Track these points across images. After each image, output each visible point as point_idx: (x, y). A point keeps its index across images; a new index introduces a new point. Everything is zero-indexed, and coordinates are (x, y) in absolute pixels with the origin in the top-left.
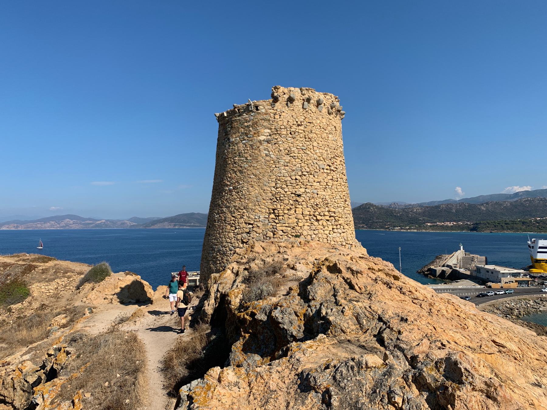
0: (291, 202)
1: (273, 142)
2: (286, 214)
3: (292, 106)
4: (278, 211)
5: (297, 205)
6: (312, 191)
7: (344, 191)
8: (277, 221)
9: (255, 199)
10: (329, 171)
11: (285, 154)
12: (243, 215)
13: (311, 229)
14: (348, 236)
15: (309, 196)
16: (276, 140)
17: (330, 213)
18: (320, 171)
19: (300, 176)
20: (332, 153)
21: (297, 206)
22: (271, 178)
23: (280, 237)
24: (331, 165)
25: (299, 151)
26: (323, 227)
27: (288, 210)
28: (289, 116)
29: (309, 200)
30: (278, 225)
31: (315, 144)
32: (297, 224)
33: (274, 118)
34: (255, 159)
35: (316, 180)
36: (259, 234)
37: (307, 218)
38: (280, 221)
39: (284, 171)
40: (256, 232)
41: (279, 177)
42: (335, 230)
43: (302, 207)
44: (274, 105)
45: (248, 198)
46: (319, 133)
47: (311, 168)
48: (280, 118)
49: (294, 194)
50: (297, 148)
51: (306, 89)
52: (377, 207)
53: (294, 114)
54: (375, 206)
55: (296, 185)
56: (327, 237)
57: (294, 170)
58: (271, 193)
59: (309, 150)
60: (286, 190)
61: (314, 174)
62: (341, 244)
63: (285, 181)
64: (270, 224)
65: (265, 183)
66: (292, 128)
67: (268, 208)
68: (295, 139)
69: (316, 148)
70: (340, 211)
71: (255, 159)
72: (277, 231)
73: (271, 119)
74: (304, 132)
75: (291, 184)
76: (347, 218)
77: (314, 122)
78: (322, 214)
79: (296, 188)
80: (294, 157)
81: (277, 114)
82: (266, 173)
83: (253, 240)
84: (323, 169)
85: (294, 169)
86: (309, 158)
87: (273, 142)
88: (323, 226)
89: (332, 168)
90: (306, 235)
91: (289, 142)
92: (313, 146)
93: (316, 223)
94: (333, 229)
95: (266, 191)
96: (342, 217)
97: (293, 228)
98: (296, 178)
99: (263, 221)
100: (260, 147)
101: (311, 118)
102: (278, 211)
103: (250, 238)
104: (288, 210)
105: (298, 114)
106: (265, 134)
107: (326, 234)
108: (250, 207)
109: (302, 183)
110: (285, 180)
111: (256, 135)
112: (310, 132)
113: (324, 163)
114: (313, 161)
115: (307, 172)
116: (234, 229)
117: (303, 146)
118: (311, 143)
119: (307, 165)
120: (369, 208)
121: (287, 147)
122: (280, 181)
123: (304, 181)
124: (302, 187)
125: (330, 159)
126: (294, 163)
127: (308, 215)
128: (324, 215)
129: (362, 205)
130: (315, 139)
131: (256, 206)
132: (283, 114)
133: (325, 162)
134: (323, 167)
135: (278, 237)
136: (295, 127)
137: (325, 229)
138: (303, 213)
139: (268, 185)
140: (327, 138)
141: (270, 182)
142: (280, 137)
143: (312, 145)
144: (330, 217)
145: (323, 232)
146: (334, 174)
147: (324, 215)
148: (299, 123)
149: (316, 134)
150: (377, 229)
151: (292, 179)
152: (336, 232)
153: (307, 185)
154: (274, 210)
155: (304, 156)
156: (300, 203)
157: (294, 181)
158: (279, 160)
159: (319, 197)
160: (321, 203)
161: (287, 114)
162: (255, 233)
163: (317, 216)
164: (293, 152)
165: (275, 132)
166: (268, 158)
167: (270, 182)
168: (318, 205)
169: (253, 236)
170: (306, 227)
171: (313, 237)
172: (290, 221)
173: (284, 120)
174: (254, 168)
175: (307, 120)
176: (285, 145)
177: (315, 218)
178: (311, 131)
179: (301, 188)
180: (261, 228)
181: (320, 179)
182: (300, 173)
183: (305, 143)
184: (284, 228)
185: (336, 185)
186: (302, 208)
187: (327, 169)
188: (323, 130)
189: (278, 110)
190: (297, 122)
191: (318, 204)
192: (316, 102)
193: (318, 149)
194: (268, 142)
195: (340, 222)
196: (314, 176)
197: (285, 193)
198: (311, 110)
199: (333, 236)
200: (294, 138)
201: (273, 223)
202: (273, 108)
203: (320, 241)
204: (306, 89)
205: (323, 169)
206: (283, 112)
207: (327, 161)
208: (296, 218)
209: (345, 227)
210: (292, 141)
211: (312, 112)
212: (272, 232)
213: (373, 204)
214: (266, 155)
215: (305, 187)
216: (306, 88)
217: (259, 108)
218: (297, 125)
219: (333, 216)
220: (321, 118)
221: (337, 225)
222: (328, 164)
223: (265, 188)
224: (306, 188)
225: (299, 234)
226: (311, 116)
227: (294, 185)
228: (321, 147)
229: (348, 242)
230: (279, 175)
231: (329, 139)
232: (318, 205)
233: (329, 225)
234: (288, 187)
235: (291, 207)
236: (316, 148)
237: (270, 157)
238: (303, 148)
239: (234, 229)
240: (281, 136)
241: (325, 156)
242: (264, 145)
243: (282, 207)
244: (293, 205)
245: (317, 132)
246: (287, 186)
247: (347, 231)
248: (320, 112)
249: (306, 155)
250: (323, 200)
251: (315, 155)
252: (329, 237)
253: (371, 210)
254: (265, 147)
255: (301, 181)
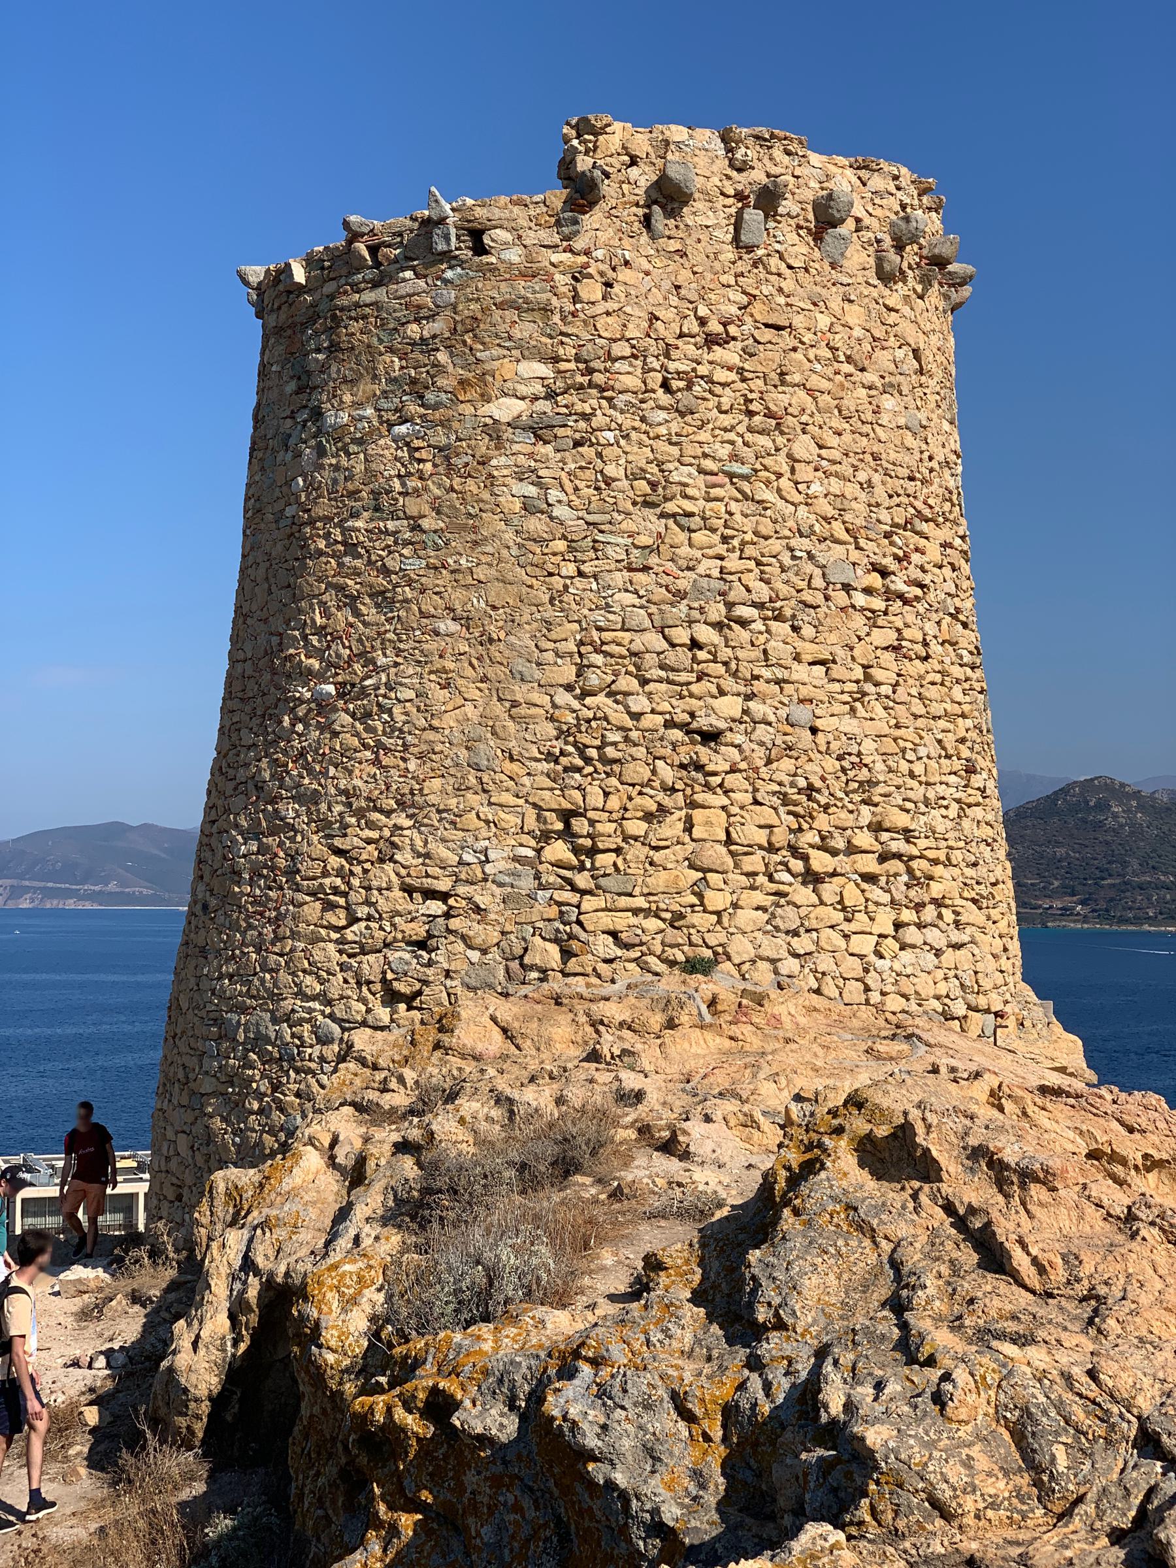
0: (667, 773)
1: (569, 432)
2: (636, 839)
3: (673, 233)
4: (592, 823)
5: (698, 788)
6: (782, 713)
7: (963, 716)
8: (583, 880)
9: (463, 754)
10: (878, 604)
11: (634, 504)
12: (394, 845)
13: (777, 929)
14: (980, 967)
15: (767, 739)
16: (582, 425)
17: (885, 836)
18: (827, 598)
19: (718, 626)
20: (896, 500)
21: (699, 798)
22: (553, 636)
23: (603, 968)
24: (893, 566)
25: (714, 486)
26: (841, 915)
27: (648, 817)
28: (659, 287)
29: (769, 762)
30: (589, 903)
31: (803, 447)
32: (700, 896)
33: (576, 299)
34: (464, 527)
35: (809, 651)
36: (484, 952)
37: (754, 862)
38: (602, 881)
39: (630, 598)
40: (463, 938)
41: (599, 629)
42: (912, 935)
43: (725, 801)
44: (576, 222)
45: (424, 747)
46: (825, 385)
47: (779, 585)
48: (604, 298)
49: (685, 727)
50: (701, 471)
51: (757, 137)
52: (1146, 803)
53: (684, 276)
54: (1137, 794)
55: (692, 677)
56: (866, 971)
57: (681, 595)
58: (552, 719)
59: (768, 483)
60: (639, 703)
61: (794, 616)
62: (943, 1013)
63: (635, 654)
64: (548, 894)
65: (520, 665)
66: (674, 354)
67: (535, 806)
68: (688, 418)
69: (810, 468)
70: (941, 826)
71: (464, 527)
72: (583, 936)
73: (555, 301)
74: (744, 380)
75: (663, 674)
76: (975, 865)
77: (798, 321)
78: (839, 843)
79: (691, 695)
80: (684, 521)
81: (590, 276)
82: (527, 610)
83: (449, 983)
84: (847, 588)
85: (682, 584)
86: (766, 527)
87: (569, 432)
88: (844, 909)
89: (899, 585)
90: (746, 957)
91: (658, 437)
92: (790, 456)
93: (803, 894)
94: (898, 926)
95: (523, 710)
96: (948, 863)
97: (677, 918)
98: (693, 639)
99: (507, 879)
100: (494, 462)
101: (782, 300)
102: (592, 823)
103: (430, 971)
104: (648, 817)
105: (709, 276)
106: (523, 390)
107: (861, 957)
108: (432, 799)
109: (725, 664)
110: (635, 647)
111: (472, 394)
112: (774, 377)
113: (855, 555)
114: (793, 543)
115: (754, 605)
116: (343, 922)
117: (735, 457)
118: (781, 440)
119: (759, 563)
120: (1102, 806)
121: (642, 463)
122: (607, 654)
123: (740, 654)
124: (727, 689)
125: (887, 535)
126: (685, 551)
127: (761, 847)
128: (852, 850)
129: (1065, 791)
130: (804, 419)
131: (469, 795)
132: (624, 275)
133: (858, 548)
134: (848, 576)
135: (589, 970)
136: (691, 350)
137: (854, 926)
138: (734, 835)
139: (537, 674)
140: (869, 416)
141: (549, 656)
142: (604, 403)
143: (783, 453)
144: (883, 858)
145: (842, 943)
146: (910, 618)
147: (852, 850)
148: (715, 327)
149: (810, 392)
150: (1146, 927)
151: (673, 645)
152: (913, 946)
153: (757, 678)
154: (566, 816)
155: (738, 517)
156: (718, 780)
157: (682, 657)
158: (600, 537)
159: (823, 748)
160: (831, 780)
161: (647, 273)
162: (460, 946)
163: (811, 851)
164: (677, 489)
165: (579, 379)
166: (536, 525)
167: (549, 656)
168: (818, 791)
169: (449, 961)
170: (747, 917)
171: (784, 971)
172: (659, 880)
173: (628, 309)
174: (459, 576)
175: (758, 309)
176: (635, 449)
177: (797, 865)
178: (782, 374)
179: (722, 693)
180: (492, 916)
181: (832, 644)
182: (717, 611)
183: (746, 444)
184: (621, 921)
185: (921, 677)
186: (723, 808)
187: (868, 591)
188: (847, 368)
189: (599, 254)
190: (703, 322)
191: (818, 784)
192: (810, 207)
193: (820, 474)
194: (539, 431)
195: (936, 889)
196: (795, 629)
197: (629, 723)
198: (782, 258)
199: (897, 966)
200: (682, 415)
201: (561, 888)
202: (567, 238)
203: (826, 991)
204: (757, 137)
205: (847, 588)
206: (627, 263)
207: (870, 546)
208: (691, 867)
209: (963, 919)
210: (675, 427)
211: (790, 267)
212: (556, 941)
213: (1122, 785)
214: (528, 507)
215: (742, 689)
216: (757, 130)
217: (486, 240)
218: (700, 340)
219: (898, 856)
220: (835, 304)
221: (923, 905)
222: (874, 559)
223: (520, 692)
224: (749, 697)
225: (708, 953)
226: (780, 290)
227: (683, 677)
228: (834, 462)
229: (982, 1002)
230: (599, 617)
231: (885, 419)
232: (818, 791)
233: (877, 904)
234: (651, 687)
235: (667, 801)
236: (810, 468)
237: (551, 518)
238: (736, 468)
239: (343, 922)
240: (610, 400)
241: (857, 514)
242: (516, 448)
243: (614, 803)
244: (673, 790)
245: (815, 382)
246: (644, 682)
247: (979, 937)
248: (833, 266)
249: (749, 507)
250: (846, 764)
251: (802, 511)
252: (872, 973)
253: (1115, 816)
254: (521, 460)
255: (725, 653)
